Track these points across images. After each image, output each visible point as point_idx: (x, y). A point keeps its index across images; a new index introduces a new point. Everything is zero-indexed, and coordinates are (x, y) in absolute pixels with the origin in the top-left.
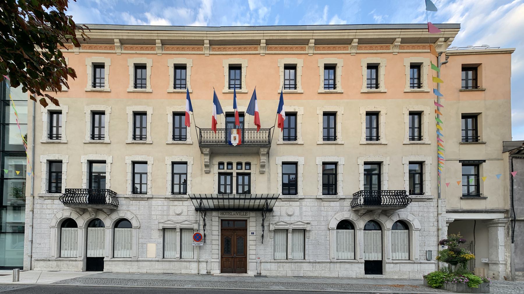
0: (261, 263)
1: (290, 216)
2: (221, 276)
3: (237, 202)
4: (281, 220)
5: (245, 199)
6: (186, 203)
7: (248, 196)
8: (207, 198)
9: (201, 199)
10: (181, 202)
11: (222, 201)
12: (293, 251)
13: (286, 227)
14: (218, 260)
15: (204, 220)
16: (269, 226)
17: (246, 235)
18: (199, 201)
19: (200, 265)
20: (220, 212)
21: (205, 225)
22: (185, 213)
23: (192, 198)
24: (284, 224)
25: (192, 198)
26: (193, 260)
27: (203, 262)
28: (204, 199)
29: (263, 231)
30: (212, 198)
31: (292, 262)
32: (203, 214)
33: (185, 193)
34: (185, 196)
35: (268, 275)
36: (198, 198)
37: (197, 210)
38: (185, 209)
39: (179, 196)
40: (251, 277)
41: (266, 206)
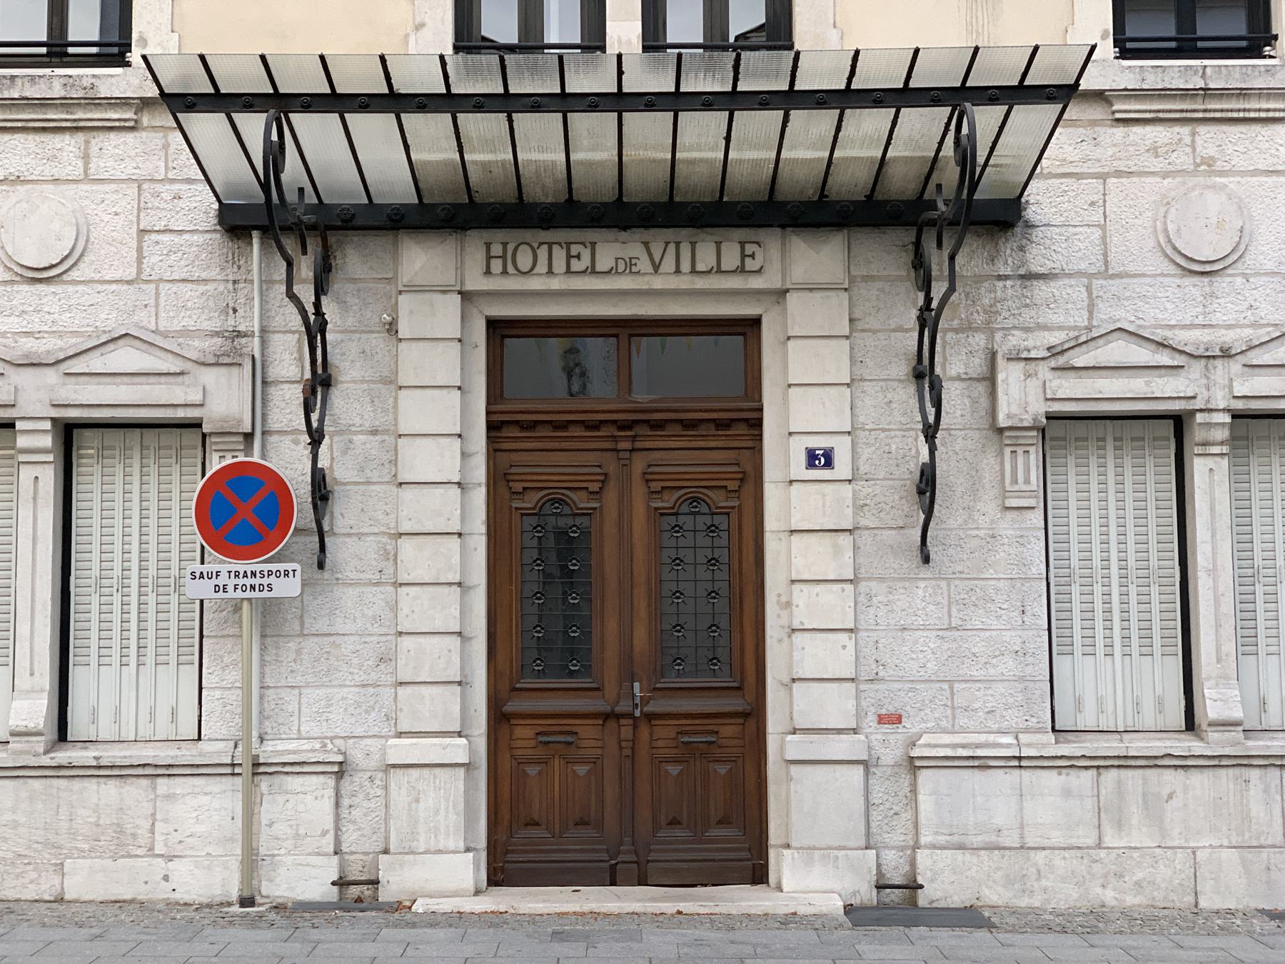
0: (913, 765)
1: (1205, 271)
2: (495, 920)
3: (649, 133)
4: (1107, 315)
5: (733, 101)
6: (121, 154)
7: (763, 73)
8: (336, 102)
9: (279, 104)
10: (68, 144)
11: (493, 123)
12: (1247, 642)
13: (1168, 390)
14: (457, 750)
15: (316, 330)
16: (990, 379)
17: (749, 480)
18: (254, 125)
19: (267, 811)
20: (475, 245)
21: (320, 383)
22: (111, 256)
23: (179, 103)
24: (1143, 355)
25: (179, 103)
26: (188, 754)
27: (297, 767)
28: (310, 103)
29: (930, 432)
30: (394, 102)
31: (1243, 762)
32: (306, 269)
33: (114, 51)
34: (112, 81)
35: (994, 895)
36: (249, 102)
37: (236, 223)
38: (112, 217)
39: (54, 82)
40: (816, 923)
41: (950, 174)
